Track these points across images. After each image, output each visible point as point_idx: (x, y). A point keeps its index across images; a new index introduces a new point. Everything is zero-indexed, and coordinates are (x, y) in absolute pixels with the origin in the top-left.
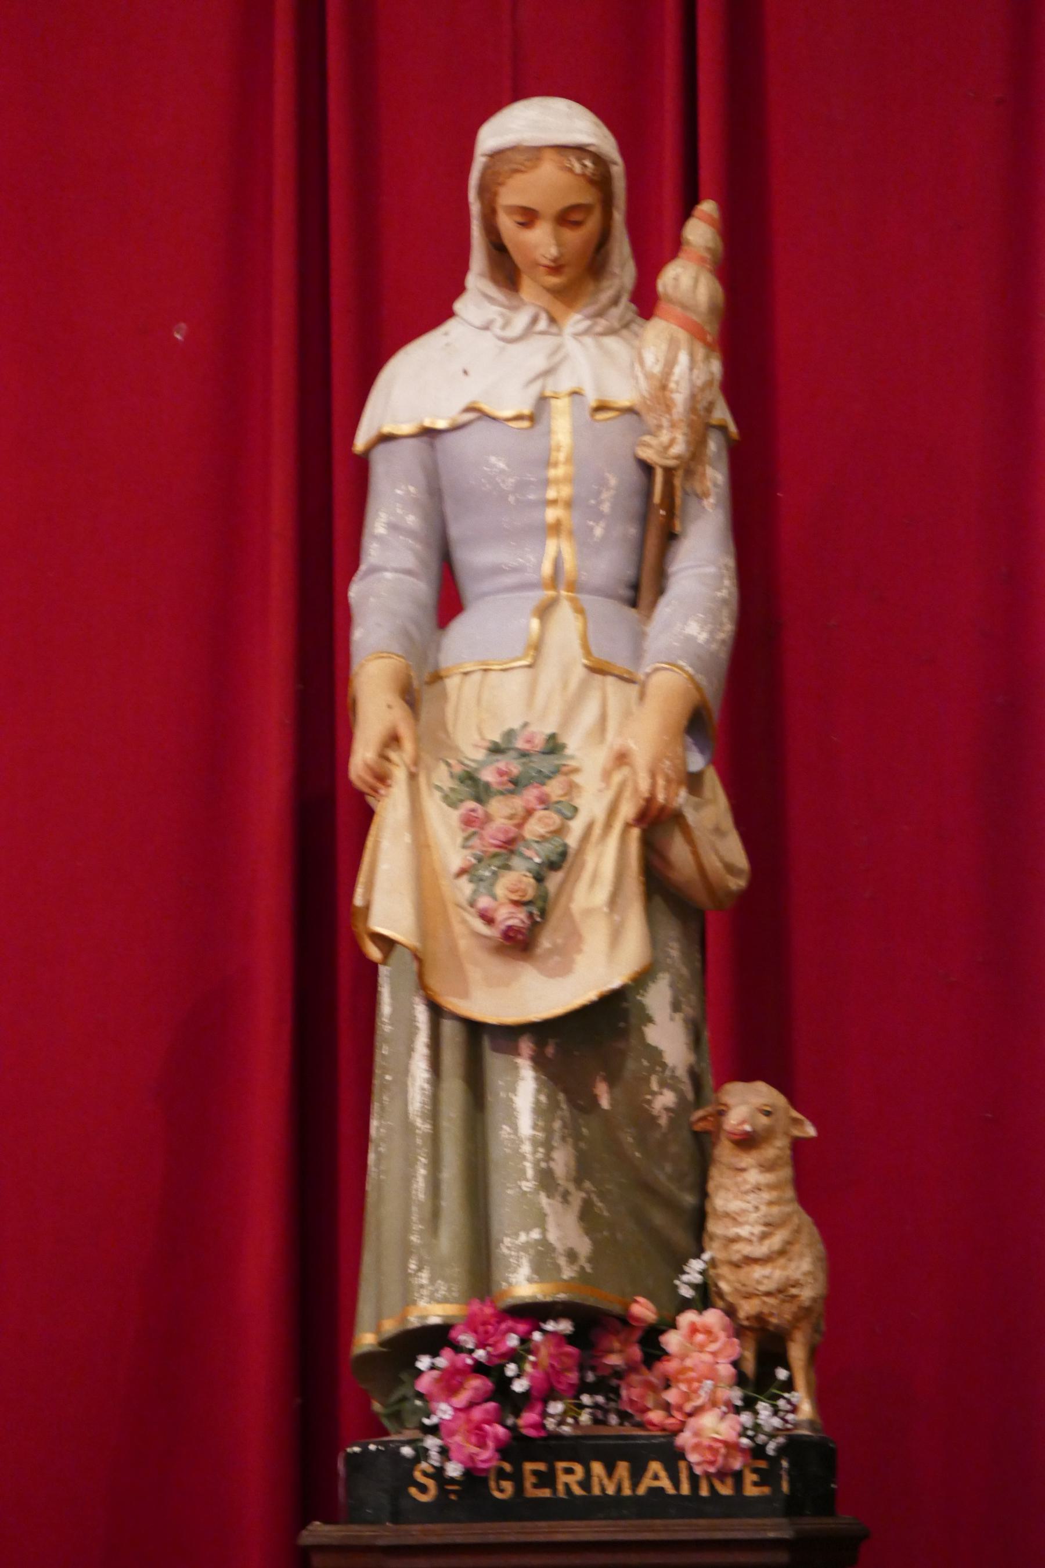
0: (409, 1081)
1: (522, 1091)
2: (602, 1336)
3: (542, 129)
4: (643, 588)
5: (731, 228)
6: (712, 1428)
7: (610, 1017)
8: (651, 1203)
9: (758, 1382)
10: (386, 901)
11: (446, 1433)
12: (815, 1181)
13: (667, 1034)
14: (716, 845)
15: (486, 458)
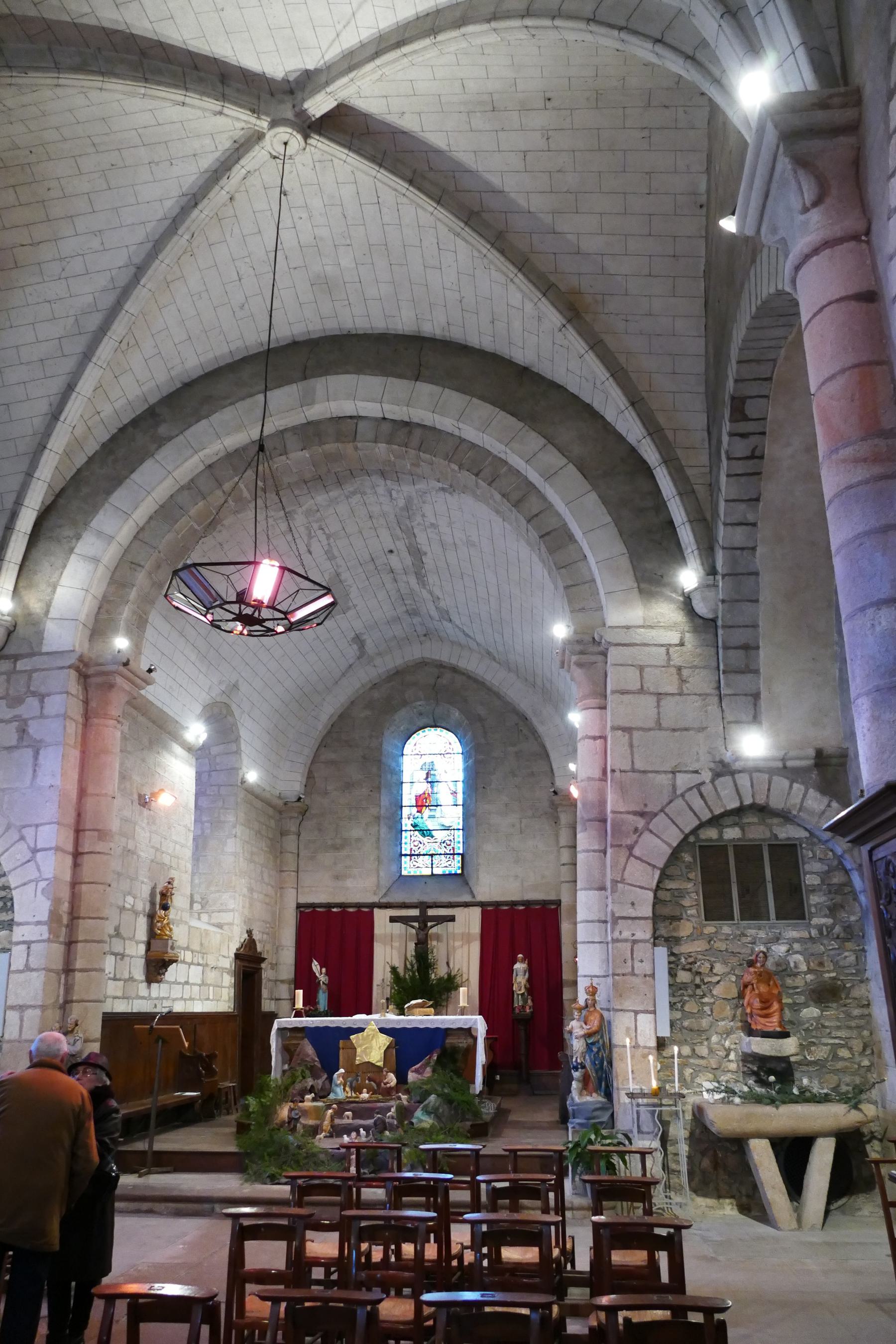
2: (523, 1007)
3: (520, 956)
8: (525, 1001)
11: (517, 1011)
12: (532, 1000)
14: (528, 986)
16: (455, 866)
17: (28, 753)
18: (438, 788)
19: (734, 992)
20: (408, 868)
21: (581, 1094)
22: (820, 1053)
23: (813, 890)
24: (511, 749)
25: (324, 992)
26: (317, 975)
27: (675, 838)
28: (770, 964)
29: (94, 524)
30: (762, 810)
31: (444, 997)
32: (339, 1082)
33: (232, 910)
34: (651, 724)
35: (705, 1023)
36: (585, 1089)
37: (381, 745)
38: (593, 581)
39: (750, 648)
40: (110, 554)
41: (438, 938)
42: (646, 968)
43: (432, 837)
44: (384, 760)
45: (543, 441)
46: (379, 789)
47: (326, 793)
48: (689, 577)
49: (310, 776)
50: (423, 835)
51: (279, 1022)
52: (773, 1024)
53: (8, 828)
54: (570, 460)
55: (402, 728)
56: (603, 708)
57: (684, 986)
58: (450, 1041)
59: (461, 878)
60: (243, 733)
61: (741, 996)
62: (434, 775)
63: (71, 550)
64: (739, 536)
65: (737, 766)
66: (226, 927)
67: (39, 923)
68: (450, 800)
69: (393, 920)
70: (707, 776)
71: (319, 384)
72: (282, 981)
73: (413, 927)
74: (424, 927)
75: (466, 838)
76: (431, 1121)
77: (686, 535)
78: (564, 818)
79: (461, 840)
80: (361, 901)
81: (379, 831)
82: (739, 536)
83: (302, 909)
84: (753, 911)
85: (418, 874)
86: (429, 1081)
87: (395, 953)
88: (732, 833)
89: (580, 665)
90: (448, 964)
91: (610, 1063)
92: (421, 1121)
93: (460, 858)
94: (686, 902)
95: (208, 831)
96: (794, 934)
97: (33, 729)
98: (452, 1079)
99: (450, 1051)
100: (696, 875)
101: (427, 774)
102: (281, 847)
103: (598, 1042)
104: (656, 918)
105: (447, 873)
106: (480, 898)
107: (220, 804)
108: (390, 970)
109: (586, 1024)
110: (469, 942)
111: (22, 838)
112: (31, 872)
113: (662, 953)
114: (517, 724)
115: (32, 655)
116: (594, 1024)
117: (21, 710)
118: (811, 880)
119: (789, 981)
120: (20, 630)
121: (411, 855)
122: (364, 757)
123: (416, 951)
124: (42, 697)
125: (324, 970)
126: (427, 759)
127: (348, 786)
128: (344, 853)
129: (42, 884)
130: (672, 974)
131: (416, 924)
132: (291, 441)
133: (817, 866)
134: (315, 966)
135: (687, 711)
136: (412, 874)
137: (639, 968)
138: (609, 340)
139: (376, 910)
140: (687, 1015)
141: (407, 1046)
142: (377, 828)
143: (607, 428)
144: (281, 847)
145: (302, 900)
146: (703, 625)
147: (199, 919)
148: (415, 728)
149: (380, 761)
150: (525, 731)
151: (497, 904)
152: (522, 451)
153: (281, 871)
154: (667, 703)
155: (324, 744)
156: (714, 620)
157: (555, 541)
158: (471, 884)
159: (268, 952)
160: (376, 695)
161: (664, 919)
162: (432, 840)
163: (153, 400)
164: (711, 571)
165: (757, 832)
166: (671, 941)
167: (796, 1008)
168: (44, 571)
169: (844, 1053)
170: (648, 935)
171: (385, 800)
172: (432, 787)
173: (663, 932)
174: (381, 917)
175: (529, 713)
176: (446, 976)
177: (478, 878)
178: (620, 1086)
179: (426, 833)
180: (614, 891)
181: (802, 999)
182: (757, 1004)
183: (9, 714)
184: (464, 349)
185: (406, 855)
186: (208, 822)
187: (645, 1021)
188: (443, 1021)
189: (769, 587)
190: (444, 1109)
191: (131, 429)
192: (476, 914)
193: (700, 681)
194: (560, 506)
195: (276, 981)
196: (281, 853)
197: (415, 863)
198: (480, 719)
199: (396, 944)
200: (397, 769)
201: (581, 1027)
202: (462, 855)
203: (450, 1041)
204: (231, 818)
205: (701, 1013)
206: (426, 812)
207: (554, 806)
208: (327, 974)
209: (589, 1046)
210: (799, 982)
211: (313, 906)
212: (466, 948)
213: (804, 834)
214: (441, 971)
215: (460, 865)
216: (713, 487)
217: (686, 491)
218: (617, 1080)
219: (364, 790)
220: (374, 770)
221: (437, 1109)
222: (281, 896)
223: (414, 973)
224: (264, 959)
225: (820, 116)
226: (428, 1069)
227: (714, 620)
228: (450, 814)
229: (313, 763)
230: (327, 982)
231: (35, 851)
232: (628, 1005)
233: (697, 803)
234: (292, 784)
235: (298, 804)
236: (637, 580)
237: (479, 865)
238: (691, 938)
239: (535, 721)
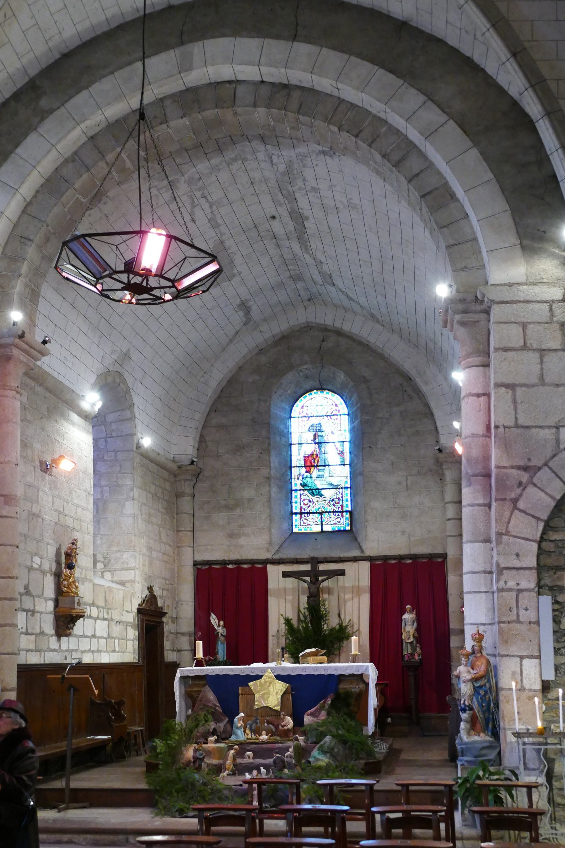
0: (405, 644)
1: (409, 645)
2: (412, 655)
3: (408, 606)
4: (413, 624)
5: (416, 612)
6: (417, 658)
7: (412, 642)
8: (414, 649)
9: (419, 656)
10: (403, 638)
11: (406, 658)
12: (421, 648)
13: (415, 642)
14: (416, 635)
15: (407, 620)
16: (344, 523)
20: (299, 525)
21: (469, 734)
24: (396, 409)
25: (222, 643)
26: (216, 627)
31: (335, 646)
32: (239, 725)
33: (134, 569)
34: (534, 380)
36: (473, 729)
37: (269, 408)
38: (475, 239)
41: (329, 591)
43: (321, 495)
44: (272, 422)
45: (422, 98)
46: (268, 451)
47: (218, 456)
49: (202, 440)
50: (313, 494)
51: (182, 671)
55: (289, 392)
58: (343, 686)
59: (350, 535)
60: (136, 400)
62: (322, 436)
66: (127, 584)
69: (286, 575)
72: (183, 634)
73: (305, 581)
74: (315, 581)
76: (327, 760)
78: (449, 475)
79: (349, 499)
80: (254, 558)
81: (269, 491)
83: (199, 567)
85: (309, 531)
86: (324, 723)
87: (289, 606)
90: (339, 615)
91: (497, 705)
92: (317, 760)
93: (348, 515)
95: (107, 495)
98: (346, 722)
99: (341, 695)
101: (315, 435)
102: (177, 508)
103: (485, 685)
105: (337, 529)
106: (368, 553)
107: (118, 469)
108: (284, 621)
109: (473, 669)
110: (359, 595)
113: (546, 601)
114: (401, 385)
116: (481, 668)
121: (301, 513)
122: (253, 420)
123: (308, 603)
125: (222, 623)
126: (315, 421)
127: (239, 449)
128: (238, 511)
131: (308, 579)
134: (214, 619)
136: (303, 531)
137: (524, 616)
139: (270, 567)
141: (303, 692)
142: (268, 489)
143: (489, 82)
144: (177, 508)
147: (103, 577)
148: (302, 391)
149: (269, 424)
151: (385, 558)
153: (178, 531)
155: (214, 409)
157: (436, 200)
159: (168, 606)
160: (263, 359)
162: (321, 499)
163: (33, 72)
170: (532, 585)
171: (275, 461)
172: (320, 448)
173: (547, 581)
174: (274, 574)
175: (413, 373)
176: (338, 627)
177: (366, 534)
178: (507, 727)
180: (499, 543)
185: (296, 513)
186: (106, 486)
187: (530, 666)
188: (336, 669)
190: (339, 749)
192: (365, 566)
195: (177, 633)
196: (177, 514)
197: (305, 521)
198: (366, 380)
199: (289, 598)
200: (285, 431)
201: (469, 672)
202: (351, 512)
203: (343, 686)
204: (128, 482)
206: (315, 473)
208: (225, 626)
209: (476, 690)
211: (209, 563)
212: (356, 600)
214: (333, 622)
215: (348, 522)
218: (504, 720)
219: (254, 452)
220: (264, 433)
221: (333, 749)
222: (179, 554)
223: (307, 624)
224: (165, 614)
226: (323, 713)
228: (337, 473)
229: (204, 427)
230: (225, 634)
232: (514, 650)
234: (185, 448)
235: (191, 467)
236: (520, 236)
237: (367, 521)
239: (419, 382)
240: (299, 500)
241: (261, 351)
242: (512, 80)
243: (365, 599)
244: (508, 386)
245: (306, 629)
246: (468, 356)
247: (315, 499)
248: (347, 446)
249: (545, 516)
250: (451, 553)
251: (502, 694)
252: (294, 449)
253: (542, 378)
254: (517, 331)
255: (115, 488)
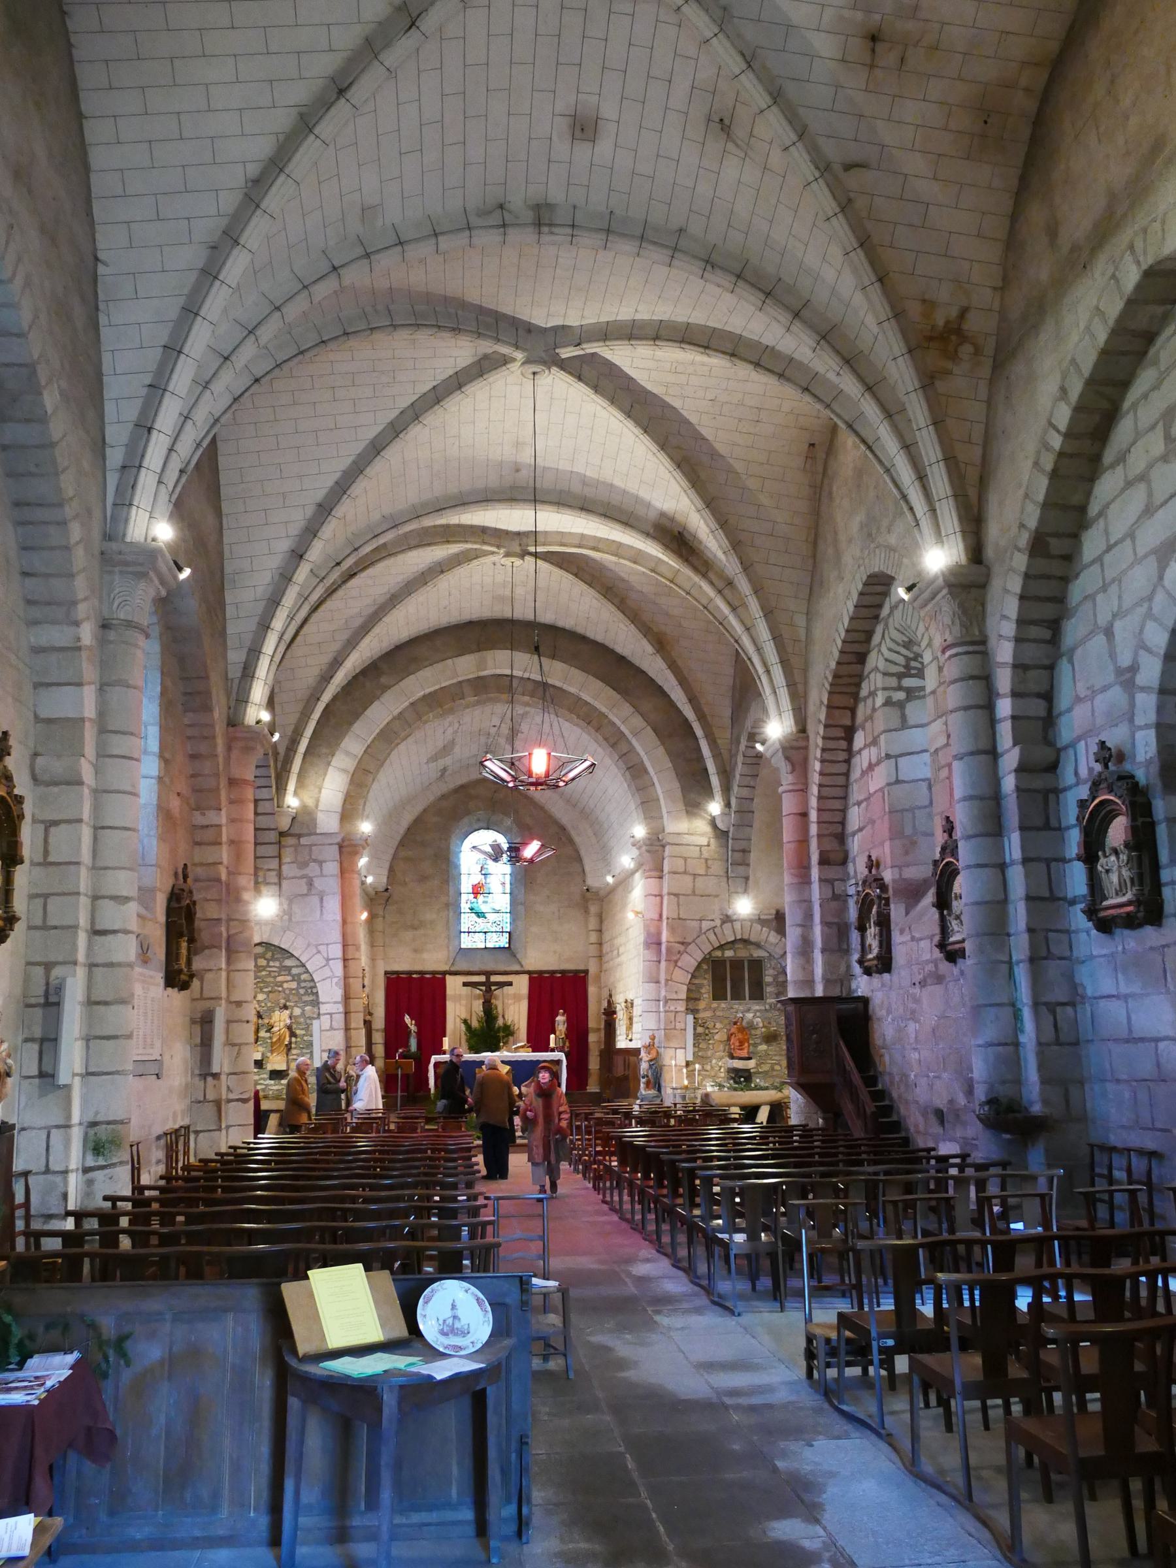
16: (503, 941)
17: (315, 900)
18: (490, 879)
19: (725, 1038)
20: (466, 942)
22: (766, 1068)
23: (769, 984)
27: (699, 956)
28: (744, 1024)
29: (342, 745)
30: (745, 942)
34: (689, 892)
35: (709, 1053)
38: (658, 800)
39: (746, 851)
40: (350, 764)
42: (679, 1026)
45: (632, 710)
48: (715, 808)
49: (391, 870)
52: (744, 1054)
53: (309, 945)
54: (649, 724)
56: (661, 878)
57: (700, 1035)
59: (509, 951)
61: (729, 1039)
63: (329, 764)
64: (745, 792)
65: (735, 917)
67: (335, 1003)
68: (500, 889)
69: (465, 984)
70: (718, 923)
71: (489, 655)
74: (488, 991)
75: (513, 921)
77: (715, 781)
78: (593, 909)
82: (745, 792)
84: (737, 996)
87: (463, 1009)
88: (729, 953)
89: (648, 851)
94: (703, 991)
96: (757, 1008)
97: (317, 883)
100: (709, 976)
104: (688, 999)
111: (319, 952)
112: (327, 972)
113: (690, 1018)
115: (309, 835)
116: (653, 1054)
117: (307, 871)
118: (768, 979)
119: (753, 1032)
120: (299, 819)
122: (435, 855)
124: (321, 863)
127: (423, 879)
128: (422, 932)
129: (335, 980)
130: (695, 1029)
132: (467, 689)
133: (771, 972)
135: (707, 885)
137: (679, 1026)
138: (680, 663)
139: (448, 977)
140: (700, 1050)
143: (672, 704)
145: (389, 969)
146: (721, 835)
150: (564, 839)
151: (541, 972)
152: (622, 715)
154: (699, 879)
155: (402, 844)
156: (727, 832)
157: (636, 772)
158: (518, 956)
161: (692, 998)
163: (375, 657)
164: (728, 805)
165: (743, 953)
166: (694, 1011)
167: (755, 1045)
168: (312, 778)
169: (777, 1067)
170: (683, 1009)
173: (690, 1006)
174: (453, 985)
175: (569, 826)
179: (480, 915)
180: (666, 985)
181: (758, 1041)
182: (737, 1044)
183: (299, 873)
184: (583, 639)
187: (680, 1052)
189: (759, 819)
191: (361, 678)
192: (526, 977)
193: (717, 868)
194: (642, 753)
199: (464, 1002)
205: (708, 1048)
206: (481, 898)
207: (584, 898)
209: (651, 1066)
210: (758, 1032)
211: (397, 973)
213: (766, 954)
216: (733, 756)
217: (717, 755)
225: (795, 744)
227: (727, 832)
228: (499, 899)
231: (328, 960)
232: (672, 1045)
233: (712, 937)
236: (686, 805)
238: (705, 1010)
239: (573, 833)
240: (467, 921)
241: (443, 797)
242: (689, 714)
243: (524, 1006)
244: (675, 895)
245: (482, 1028)
246: (650, 870)
247: (480, 920)
248: (508, 878)
249: (691, 970)
250: (593, 970)
251: (665, 1069)
252: (464, 879)
253: (694, 891)
254: (681, 862)
255: (1007, 1117)
